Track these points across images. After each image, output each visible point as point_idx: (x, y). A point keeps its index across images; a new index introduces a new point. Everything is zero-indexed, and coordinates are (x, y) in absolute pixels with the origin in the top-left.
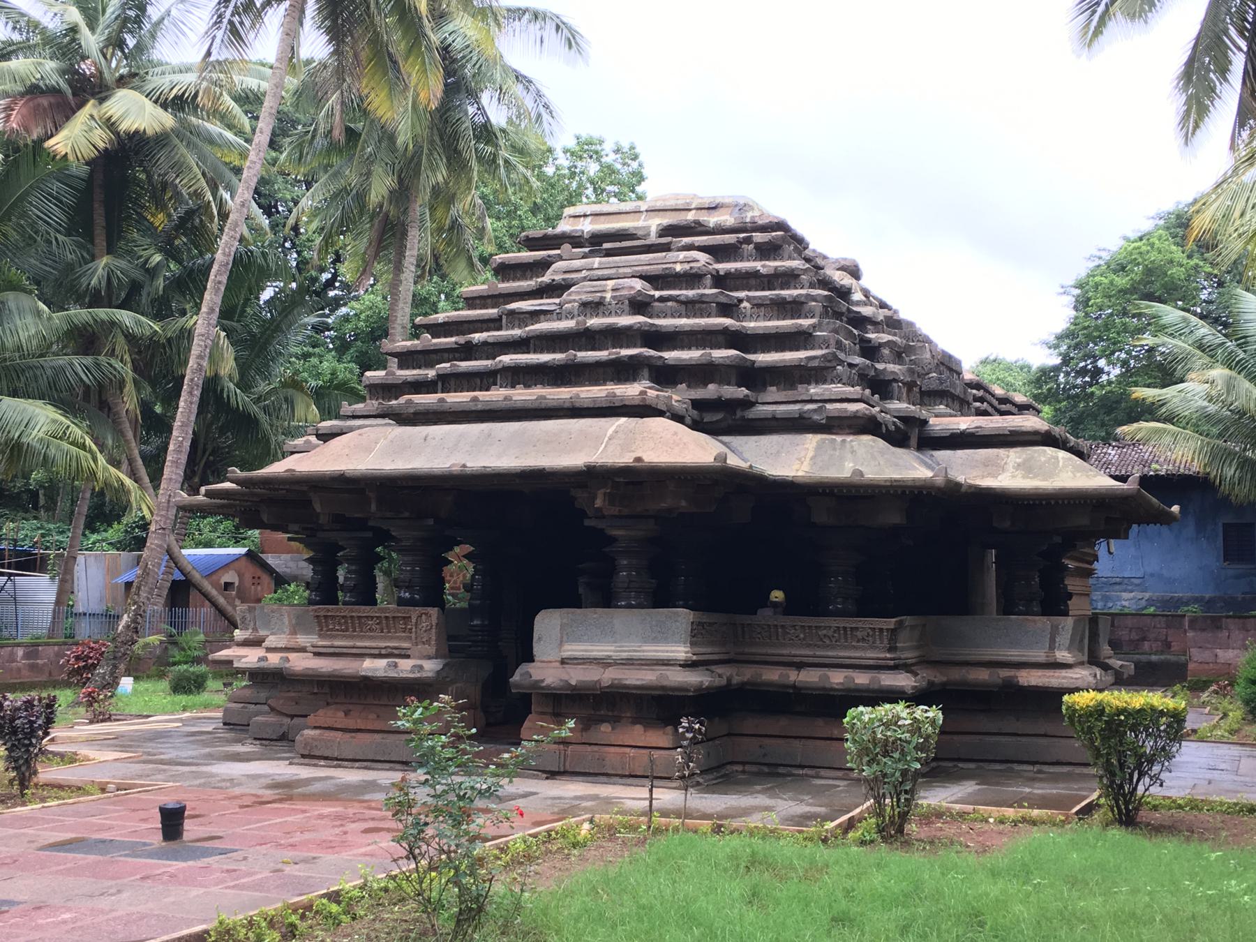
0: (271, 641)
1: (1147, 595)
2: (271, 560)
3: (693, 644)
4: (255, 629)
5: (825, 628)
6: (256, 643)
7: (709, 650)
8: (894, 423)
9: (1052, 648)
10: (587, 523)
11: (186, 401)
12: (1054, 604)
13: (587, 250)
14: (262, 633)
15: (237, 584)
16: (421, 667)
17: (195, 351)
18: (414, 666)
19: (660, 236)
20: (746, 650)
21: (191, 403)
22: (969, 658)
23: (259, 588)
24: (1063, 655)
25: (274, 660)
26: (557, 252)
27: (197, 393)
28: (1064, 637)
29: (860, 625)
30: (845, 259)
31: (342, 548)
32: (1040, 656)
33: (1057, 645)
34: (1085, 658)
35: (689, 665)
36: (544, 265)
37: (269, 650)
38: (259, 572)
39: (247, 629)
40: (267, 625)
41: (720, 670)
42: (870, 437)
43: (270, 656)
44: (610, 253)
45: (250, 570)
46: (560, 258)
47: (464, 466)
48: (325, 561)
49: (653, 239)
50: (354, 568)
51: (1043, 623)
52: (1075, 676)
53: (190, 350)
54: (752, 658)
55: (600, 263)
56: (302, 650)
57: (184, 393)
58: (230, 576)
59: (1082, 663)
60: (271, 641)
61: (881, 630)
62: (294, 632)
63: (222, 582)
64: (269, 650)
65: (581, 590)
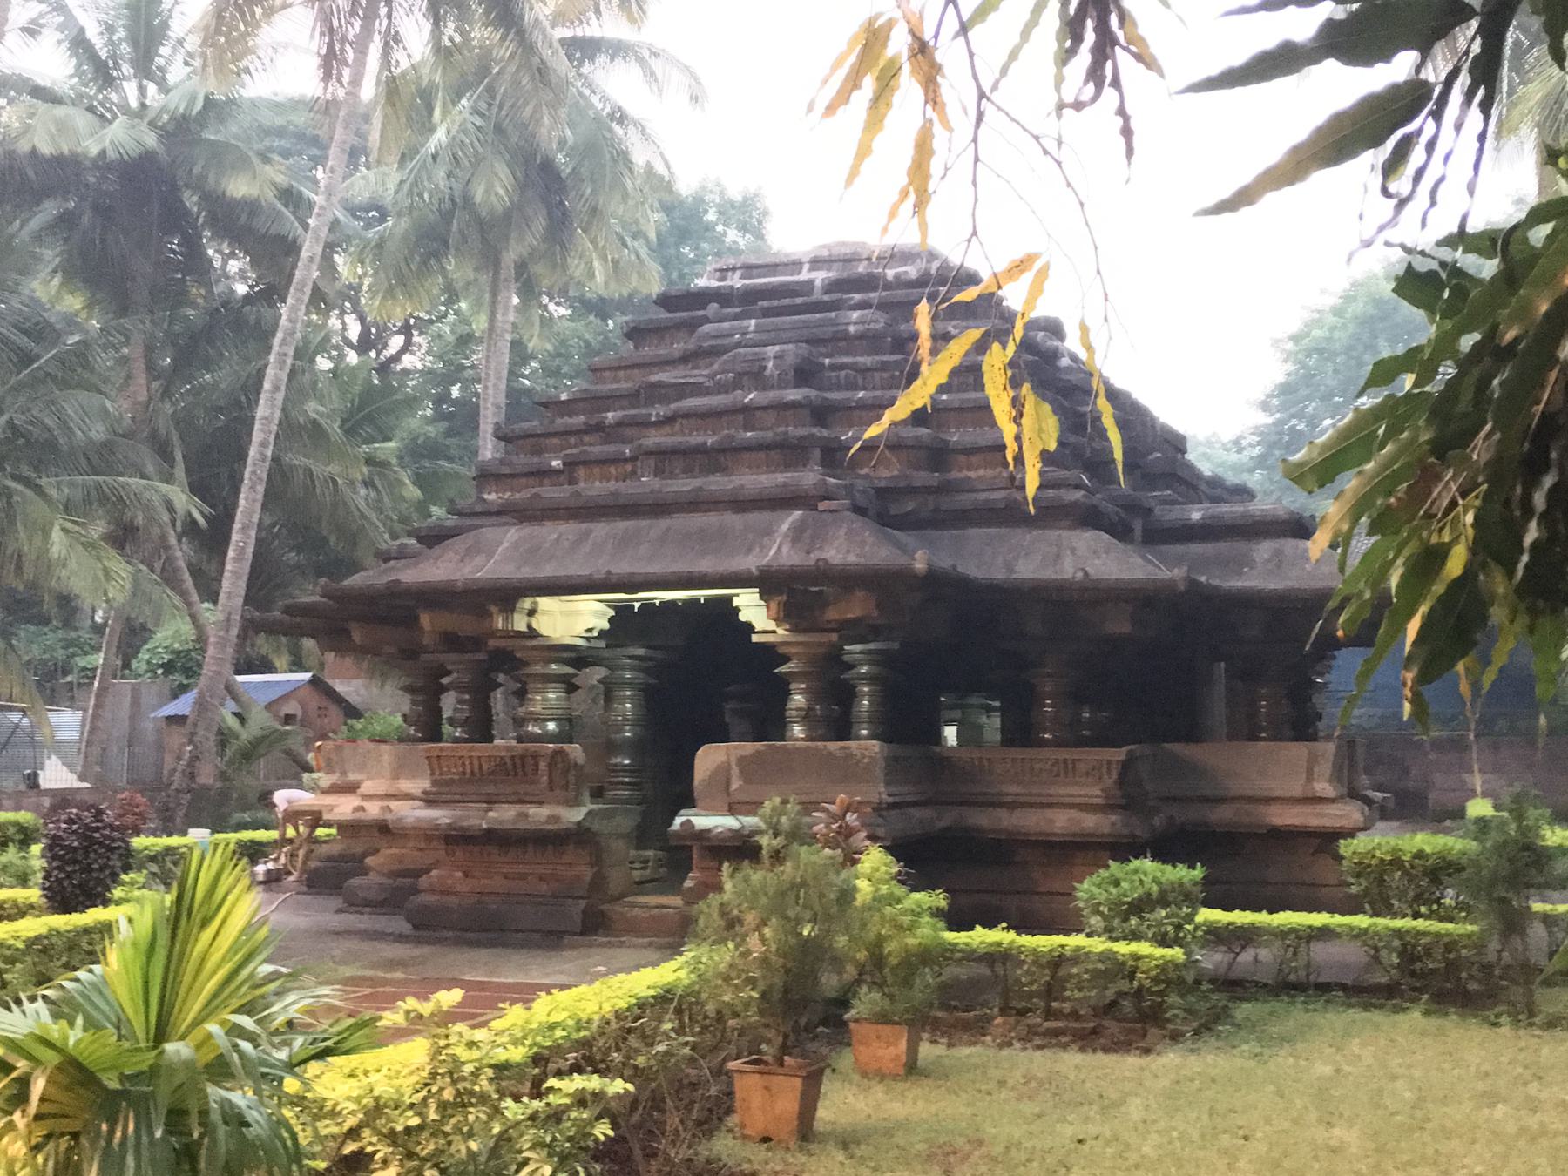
0: (368, 787)
1: (1379, 712)
2: (340, 687)
3: (887, 784)
4: (344, 773)
5: (1041, 760)
6: (351, 788)
7: (905, 789)
8: (1117, 514)
9: (1310, 777)
10: (755, 638)
11: (246, 499)
12: (1303, 727)
13: (738, 310)
14: (353, 777)
15: (299, 718)
16: (362, 809)
17: (257, 436)
18: (382, 808)
19: (826, 293)
20: (1052, 791)
21: (254, 501)
22: (1277, 793)
23: (326, 721)
24: (1324, 788)
25: (373, 810)
26: (701, 313)
27: (261, 488)
28: (1325, 768)
29: (1084, 756)
30: (844, 244)
31: (449, 673)
32: (1296, 789)
33: (1315, 776)
34: (1345, 791)
35: (429, 800)
36: (691, 326)
37: (366, 797)
38: (325, 702)
39: (334, 772)
40: (362, 768)
41: (917, 813)
42: (1107, 536)
43: (366, 805)
44: (767, 313)
45: (315, 701)
46: (706, 320)
47: (609, 572)
48: (427, 692)
49: (817, 295)
50: (420, 698)
51: (1299, 750)
52: (1338, 813)
53: (250, 435)
54: (1062, 800)
55: (756, 325)
56: (408, 797)
57: (244, 489)
58: (292, 708)
59: (1342, 797)
60: (368, 787)
61: (1109, 762)
62: (396, 776)
63: (282, 714)
64: (366, 797)
65: (727, 719)
